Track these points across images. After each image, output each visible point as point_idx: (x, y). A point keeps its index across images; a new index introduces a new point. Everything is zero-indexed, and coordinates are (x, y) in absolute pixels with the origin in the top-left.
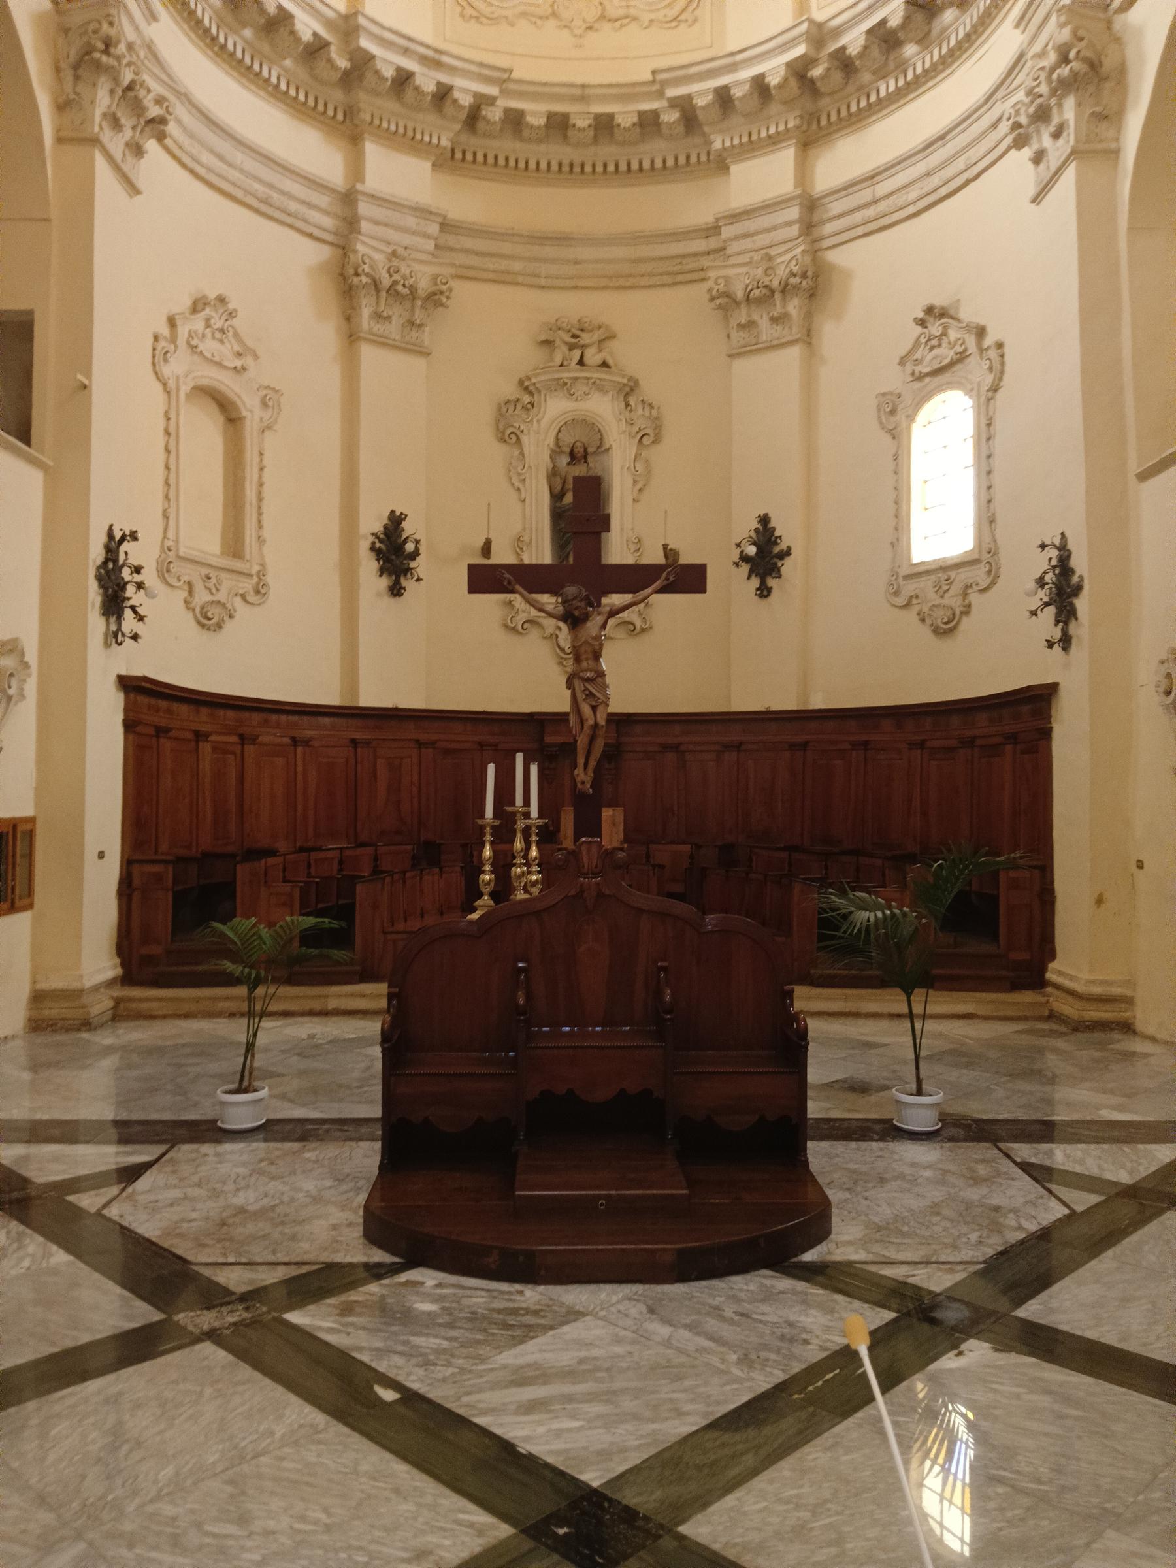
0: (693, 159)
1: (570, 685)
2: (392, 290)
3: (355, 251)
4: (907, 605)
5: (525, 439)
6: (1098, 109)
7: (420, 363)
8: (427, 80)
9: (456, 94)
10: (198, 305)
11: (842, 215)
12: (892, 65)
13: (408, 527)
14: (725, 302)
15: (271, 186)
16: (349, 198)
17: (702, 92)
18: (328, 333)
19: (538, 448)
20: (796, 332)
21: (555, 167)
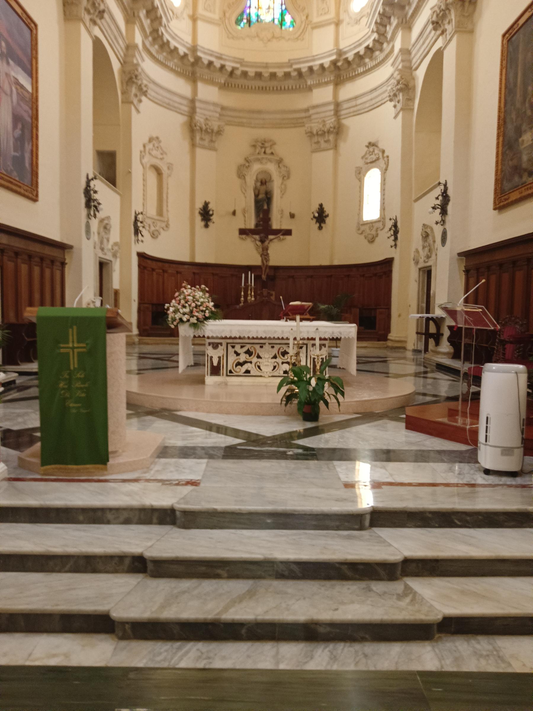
0: (302, 86)
1: (261, 256)
2: (206, 131)
3: (195, 119)
4: (362, 233)
5: (246, 177)
6: (408, 97)
7: (213, 153)
8: (218, 64)
9: (227, 67)
10: (151, 140)
11: (346, 109)
12: (362, 64)
13: (210, 206)
14: (311, 134)
15: (170, 99)
16: (193, 101)
17: (304, 67)
18: (186, 145)
19: (251, 181)
20: (332, 145)
21: (257, 88)
